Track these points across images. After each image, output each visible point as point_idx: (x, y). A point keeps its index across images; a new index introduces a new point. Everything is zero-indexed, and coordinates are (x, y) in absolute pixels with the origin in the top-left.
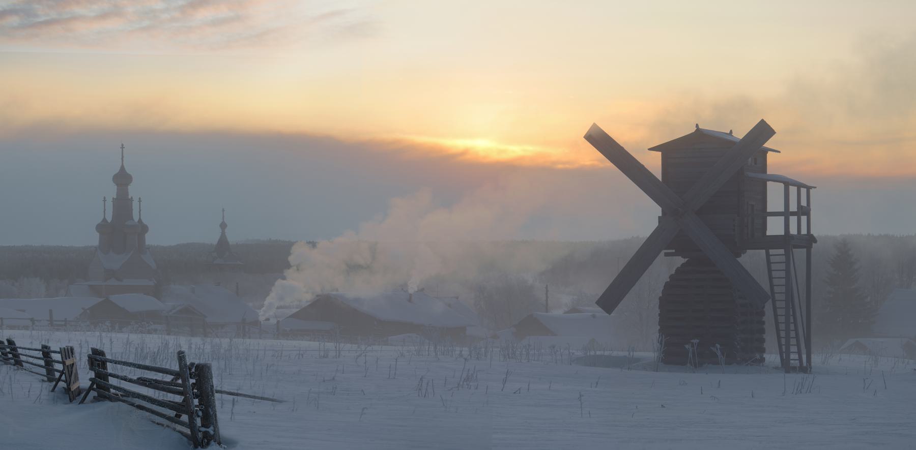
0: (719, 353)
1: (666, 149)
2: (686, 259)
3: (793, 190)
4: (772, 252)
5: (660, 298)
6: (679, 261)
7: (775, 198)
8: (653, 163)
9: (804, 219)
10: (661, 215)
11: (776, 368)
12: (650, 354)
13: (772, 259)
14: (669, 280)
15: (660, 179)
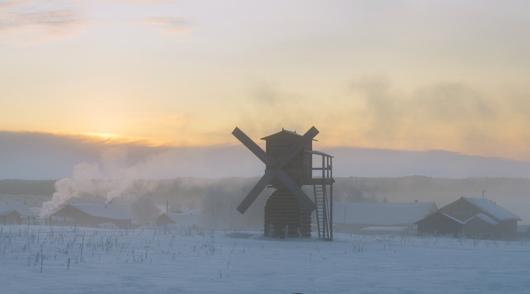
0: (299, 232)
1: (268, 139)
2: (276, 189)
3: (326, 158)
4: (316, 186)
5: (265, 207)
6: (273, 190)
7: (317, 161)
8: (263, 145)
9: (330, 171)
10: (265, 169)
11: (317, 239)
12: (260, 232)
13: (317, 189)
14: (269, 199)
15: (265, 152)
